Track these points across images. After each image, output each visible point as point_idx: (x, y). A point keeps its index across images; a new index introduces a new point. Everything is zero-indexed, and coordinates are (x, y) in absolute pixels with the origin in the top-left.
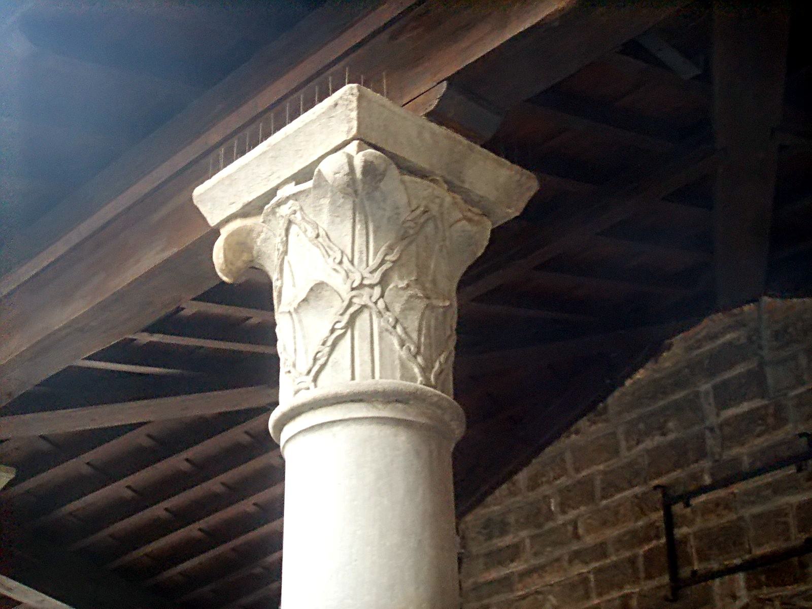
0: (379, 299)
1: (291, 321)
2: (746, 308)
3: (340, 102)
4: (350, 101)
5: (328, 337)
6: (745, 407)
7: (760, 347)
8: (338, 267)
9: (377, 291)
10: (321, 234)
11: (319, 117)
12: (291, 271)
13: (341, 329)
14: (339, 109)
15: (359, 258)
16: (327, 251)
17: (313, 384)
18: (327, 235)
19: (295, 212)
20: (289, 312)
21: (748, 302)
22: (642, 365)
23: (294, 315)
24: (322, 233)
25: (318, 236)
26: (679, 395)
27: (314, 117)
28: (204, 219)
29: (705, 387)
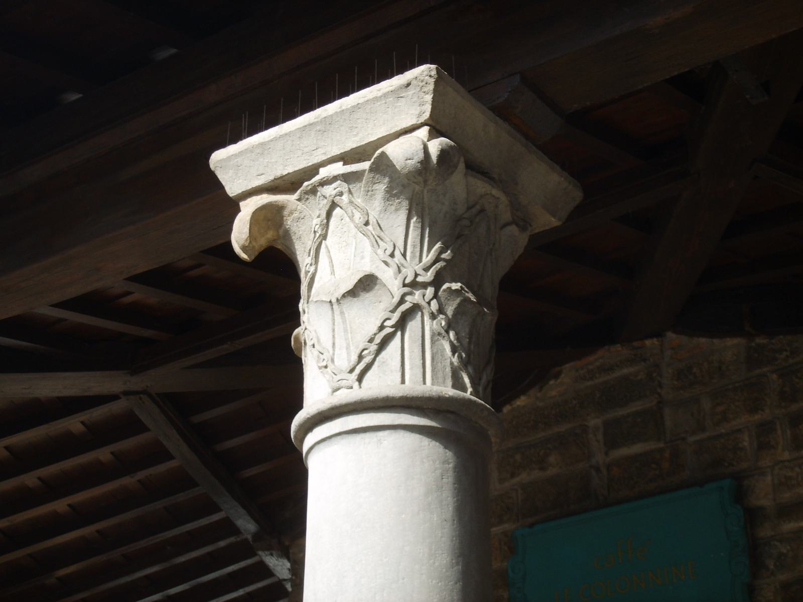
0: (432, 299)
1: (330, 312)
2: (648, 342)
3: (414, 82)
4: (426, 84)
5: (375, 334)
6: (637, 448)
7: (660, 385)
8: (389, 260)
9: (430, 291)
10: (371, 222)
11: (385, 95)
12: (330, 258)
13: (392, 327)
14: (411, 91)
15: (412, 252)
16: (376, 241)
17: (357, 383)
18: (378, 223)
19: (341, 194)
20: (330, 302)
21: (651, 336)
22: (523, 392)
23: (335, 306)
24: (372, 220)
25: (367, 224)
26: (563, 428)
27: (380, 94)
28: (221, 187)
29: (594, 422)
